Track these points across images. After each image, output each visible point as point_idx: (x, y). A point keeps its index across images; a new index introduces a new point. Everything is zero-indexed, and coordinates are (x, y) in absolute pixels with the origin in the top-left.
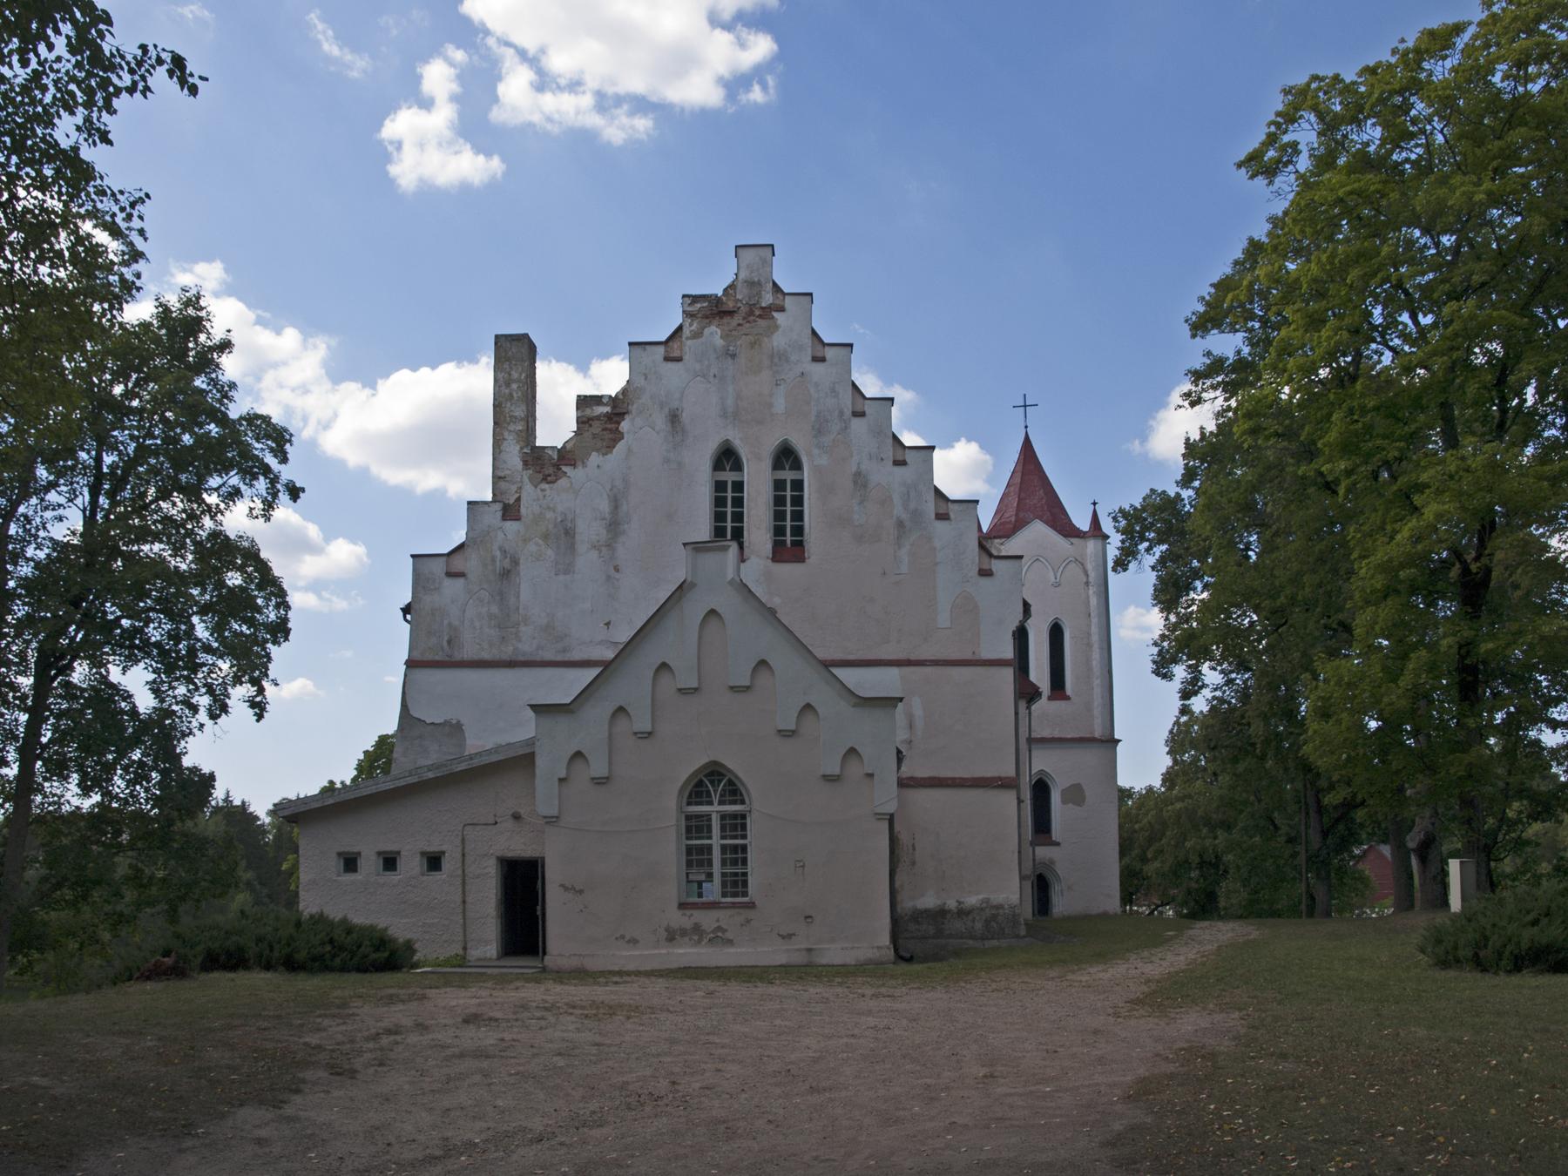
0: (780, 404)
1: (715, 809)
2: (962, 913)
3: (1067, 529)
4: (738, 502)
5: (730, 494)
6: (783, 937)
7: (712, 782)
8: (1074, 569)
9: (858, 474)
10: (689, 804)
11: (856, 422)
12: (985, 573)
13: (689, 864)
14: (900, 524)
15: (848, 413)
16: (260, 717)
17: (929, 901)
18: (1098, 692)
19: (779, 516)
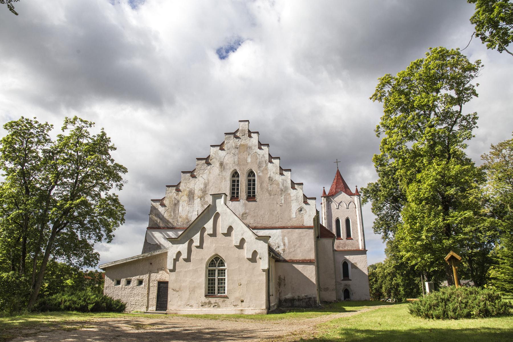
0: (249, 160)
1: (217, 269)
2: (299, 300)
4: (238, 185)
5: (252, 183)
7: (216, 260)
9: (270, 177)
10: (209, 266)
13: (209, 284)
16: (237, 247)
17: (289, 296)
19: (249, 189)
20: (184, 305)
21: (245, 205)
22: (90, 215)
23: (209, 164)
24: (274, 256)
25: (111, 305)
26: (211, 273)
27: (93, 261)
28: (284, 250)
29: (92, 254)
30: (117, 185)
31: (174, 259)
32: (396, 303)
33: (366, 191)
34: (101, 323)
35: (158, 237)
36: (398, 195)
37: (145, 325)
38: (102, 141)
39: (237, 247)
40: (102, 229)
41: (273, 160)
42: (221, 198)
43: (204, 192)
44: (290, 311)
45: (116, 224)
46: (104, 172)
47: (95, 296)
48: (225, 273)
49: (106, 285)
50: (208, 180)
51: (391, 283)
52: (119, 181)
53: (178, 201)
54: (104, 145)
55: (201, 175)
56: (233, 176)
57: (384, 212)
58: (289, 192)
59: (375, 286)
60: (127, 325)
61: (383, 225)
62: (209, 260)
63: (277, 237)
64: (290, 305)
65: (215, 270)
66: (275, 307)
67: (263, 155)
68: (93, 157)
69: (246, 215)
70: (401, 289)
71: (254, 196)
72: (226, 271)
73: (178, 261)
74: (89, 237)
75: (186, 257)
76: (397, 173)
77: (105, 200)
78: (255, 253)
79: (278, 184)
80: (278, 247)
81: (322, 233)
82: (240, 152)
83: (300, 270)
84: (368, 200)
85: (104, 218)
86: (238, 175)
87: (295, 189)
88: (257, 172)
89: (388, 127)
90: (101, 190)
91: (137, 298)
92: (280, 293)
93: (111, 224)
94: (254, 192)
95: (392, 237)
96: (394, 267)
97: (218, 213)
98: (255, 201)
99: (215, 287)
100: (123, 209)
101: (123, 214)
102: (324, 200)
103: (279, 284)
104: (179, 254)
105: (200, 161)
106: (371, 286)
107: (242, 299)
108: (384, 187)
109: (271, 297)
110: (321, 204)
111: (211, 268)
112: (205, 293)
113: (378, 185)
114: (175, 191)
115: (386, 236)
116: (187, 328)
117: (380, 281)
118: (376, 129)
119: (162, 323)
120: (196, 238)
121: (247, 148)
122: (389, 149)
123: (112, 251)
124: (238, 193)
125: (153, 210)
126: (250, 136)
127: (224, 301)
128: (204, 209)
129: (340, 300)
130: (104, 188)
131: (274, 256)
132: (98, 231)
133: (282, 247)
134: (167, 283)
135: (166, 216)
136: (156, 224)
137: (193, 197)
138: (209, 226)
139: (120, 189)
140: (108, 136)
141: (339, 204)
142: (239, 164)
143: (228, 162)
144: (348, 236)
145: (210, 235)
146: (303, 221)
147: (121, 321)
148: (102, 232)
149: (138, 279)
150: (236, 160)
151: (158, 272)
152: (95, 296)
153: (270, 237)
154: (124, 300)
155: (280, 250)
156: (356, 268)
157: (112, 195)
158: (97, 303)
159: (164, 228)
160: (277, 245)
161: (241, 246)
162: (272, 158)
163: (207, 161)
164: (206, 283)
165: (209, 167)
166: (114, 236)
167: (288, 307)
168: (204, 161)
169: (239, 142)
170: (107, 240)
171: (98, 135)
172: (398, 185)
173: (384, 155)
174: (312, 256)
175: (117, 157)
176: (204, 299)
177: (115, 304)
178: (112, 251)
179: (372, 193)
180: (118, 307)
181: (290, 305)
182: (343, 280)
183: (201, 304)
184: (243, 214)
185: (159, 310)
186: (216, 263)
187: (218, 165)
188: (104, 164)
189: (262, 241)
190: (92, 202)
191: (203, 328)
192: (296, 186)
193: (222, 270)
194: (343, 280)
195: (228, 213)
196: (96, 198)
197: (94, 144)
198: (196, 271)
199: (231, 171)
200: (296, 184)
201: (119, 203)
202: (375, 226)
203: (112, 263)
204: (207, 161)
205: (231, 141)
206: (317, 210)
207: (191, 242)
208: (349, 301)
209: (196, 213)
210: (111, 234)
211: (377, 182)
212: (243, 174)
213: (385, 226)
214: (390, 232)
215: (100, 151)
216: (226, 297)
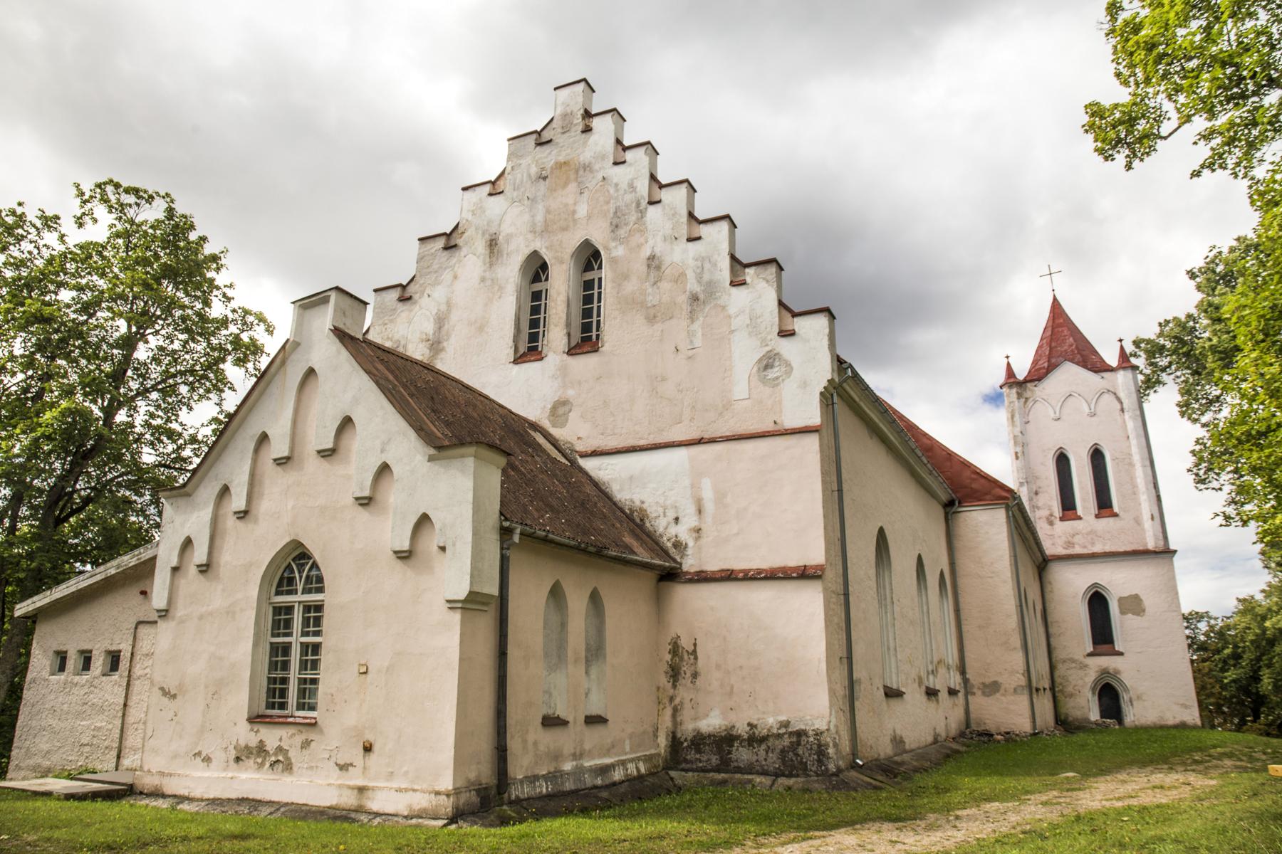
0: (582, 210)
2: (754, 740)
3: (1099, 367)
8: (1108, 398)
9: (652, 258)
10: (278, 593)
11: (652, 208)
12: (786, 334)
14: (695, 298)
15: (644, 203)
17: (712, 722)
18: (1146, 508)
33: (1154, 350)
55: (428, 291)
65: (289, 609)
69: (566, 408)
84: (1164, 377)
92: (675, 711)
107: (369, 737)
121: (577, 171)
133: (689, 521)
142: (546, 230)
150: (539, 218)
160: (671, 515)
174: (814, 552)
176: (245, 735)
182: (1090, 655)
184: (554, 409)
194: (1090, 655)
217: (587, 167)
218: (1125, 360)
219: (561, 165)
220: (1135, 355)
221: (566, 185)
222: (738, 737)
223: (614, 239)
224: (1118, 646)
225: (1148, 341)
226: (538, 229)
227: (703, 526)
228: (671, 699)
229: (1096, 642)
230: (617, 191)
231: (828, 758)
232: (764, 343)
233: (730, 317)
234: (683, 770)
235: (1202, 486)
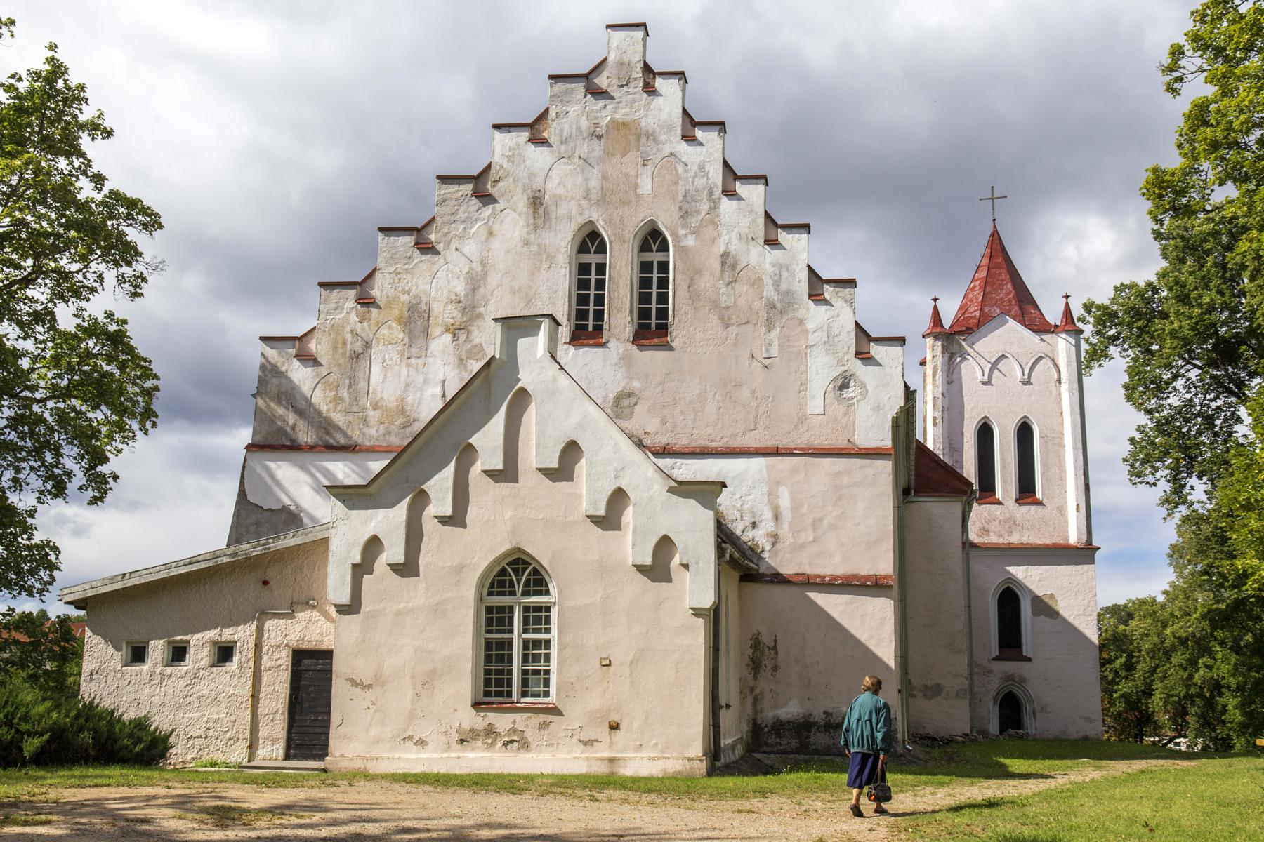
0: (646, 185)
4: (600, 285)
6: (585, 743)
7: (516, 571)
9: (725, 255)
10: (490, 594)
13: (488, 659)
16: (597, 521)
17: (791, 710)
19: (645, 298)
20: (393, 738)
21: (626, 361)
22: (16, 396)
23: (485, 198)
24: (739, 562)
25: (112, 737)
26: (495, 619)
27: (33, 572)
28: (775, 538)
29: (29, 548)
30: (122, 280)
31: (355, 566)
32: (1205, 753)
33: (1105, 316)
34: (82, 804)
35: (294, 482)
36: (1236, 335)
37: (248, 811)
38: (50, 97)
39: (597, 521)
40: (66, 449)
41: (739, 187)
42: (534, 331)
43: (469, 310)
44: (795, 768)
45: (122, 430)
46: (68, 226)
47: (48, 704)
48: (548, 621)
49: (88, 665)
50: (483, 263)
51: (1191, 677)
52: (129, 264)
53: (368, 345)
54: (61, 114)
56: (583, 249)
57: (1174, 401)
58: (801, 313)
59: (1123, 687)
60: (178, 812)
61: (1166, 453)
62: (489, 569)
63: (749, 490)
64: (794, 743)
65: (511, 609)
66: (739, 750)
67: (701, 167)
68: (18, 162)
69: (633, 400)
70: (1230, 702)
71: (663, 329)
72: (554, 614)
73: (371, 572)
74: (15, 480)
75: (400, 558)
76: (1243, 246)
77: (75, 336)
78: (665, 545)
79: (757, 283)
80: (754, 525)
81: (925, 478)
82: (608, 154)
83: (835, 615)
84: (1113, 350)
85: (74, 409)
86: (603, 243)
87: (826, 302)
88: (674, 235)
89: (1219, 51)
90: (58, 296)
91: (212, 713)
92: (756, 700)
93: (104, 429)
94: (663, 313)
95: (1204, 498)
96: (1203, 617)
97: (523, 391)
98: (667, 346)
99: (510, 672)
100: (148, 374)
101: (149, 393)
102: (932, 350)
103: (755, 666)
104: (373, 545)
105: (453, 188)
106: (1108, 687)
107: (615, 717)
108: (1183, 299)
109: (723, 713)
110: (923, 363)
111: (497, 600)
112: (475, 694)
113: (1155, 291)
114: (353, 304)
115: (1177, 496)
116: (408, 824)
117: (1142, 667)
118: (1167, 61)
119: (315, 807)
120: (440, 486)
121: (638, 138)
122: (1215, 146)
123: (99, 539)
124: (599, 315)
125: (271, 382)
126: (649, 89)
127: (544, 726)
128: (467, 377)
129: (985, 733)
130: (67, 288)
131: (739, 562)
132: (49, 458)
133: (767, 526)
134: (327, 655)
135: (320, 399)
136: (282, 431)
137: (426, 331)
138: (488, 441)
139: (135, 295)
140: (74, 80)
141: (994, 366)
142: (603, 200)
143: (561, 191)
144: (1026, 490)
145: (494, 475)
146: (850, 427)
147: (154, 797)
148: (68, 463)
149: (215, 643)
150: (594, 184)
151: (291, 615)
152: (48, 704)
153: (724, 485)
154: (161, 722)
155: (759, 537)
156: (1053, 614)
157: (101, 319)
158: (58, 734)
159: (312, 448)
160: (748, 519)
161: (609, 520)
162: (737, 178)
163: (481, 186)
164: (476, 657)
165: (487, 211)
166: (116, 478)
167: (784, 752)
168: (468, 188)
169: (606, 113)
170: (90, 493)
171: (36, 75)
172: (1243, 293)
173: (1191, 170)
174: (884, 564)
175: (115, 164)
176: (469, 718)
177: (130, 736)
178: (99, 539)
179: (1130, 324)
180: (138, 748)
181: (794, 743)
182: (994, 659)
183: (456, 737)
184: (618, 399)
185: (296, 757)
186: (516, 576)
187: (521, 201)
188: (65, 194)
189: (692, 501)
190: (22, 345)
191: (471, 822)
192: (828, 291)
193: (538, 608)
194: (994, 659)
195: (566, 390)
196: (40, 329)
197: (19, 110)
198: (438, 610)
199: (574, 226)
200: (829, 282)
201: (130, 350)
202: (1134, 455)
203: (113, 579)
204: (481, 186)
205: (574, 109)
206: (907, 387)
207: (421, 499)
208: (1020, 738)
209: (438, 390)
210: (104, 469)
211: (1154, 279)
212: (623, 241)
213: (1174, 454)
214: (1194, 481)
215: (44, 139)
216: (554, 711)
217: (650, 136)
218: (1069, 324)
219: (619, 126)
220: (1081, 320)
221: (625, 153)
222: (815, 724)
223: (684, 227)
224: (1027, 649)
225: (1099, 307)
226: (594, 196)
227: (780, 532)
228: (752, 689)
229: (1002, 644)
230: (686, 171)
231: (897, 742)
232: (840, 362)
233: (807, 332)
234: (764, 752)
235: (1137, 480)
